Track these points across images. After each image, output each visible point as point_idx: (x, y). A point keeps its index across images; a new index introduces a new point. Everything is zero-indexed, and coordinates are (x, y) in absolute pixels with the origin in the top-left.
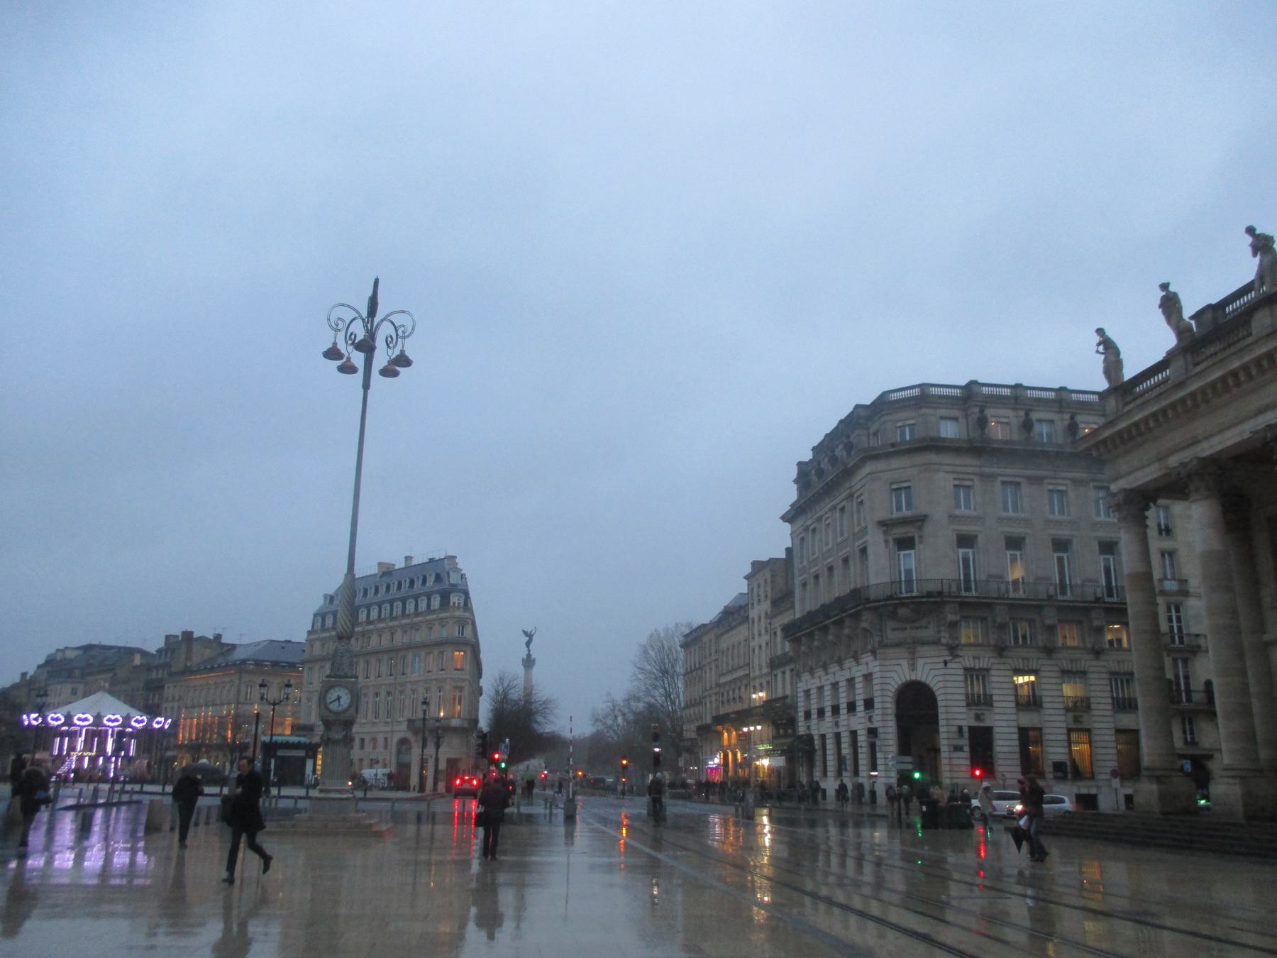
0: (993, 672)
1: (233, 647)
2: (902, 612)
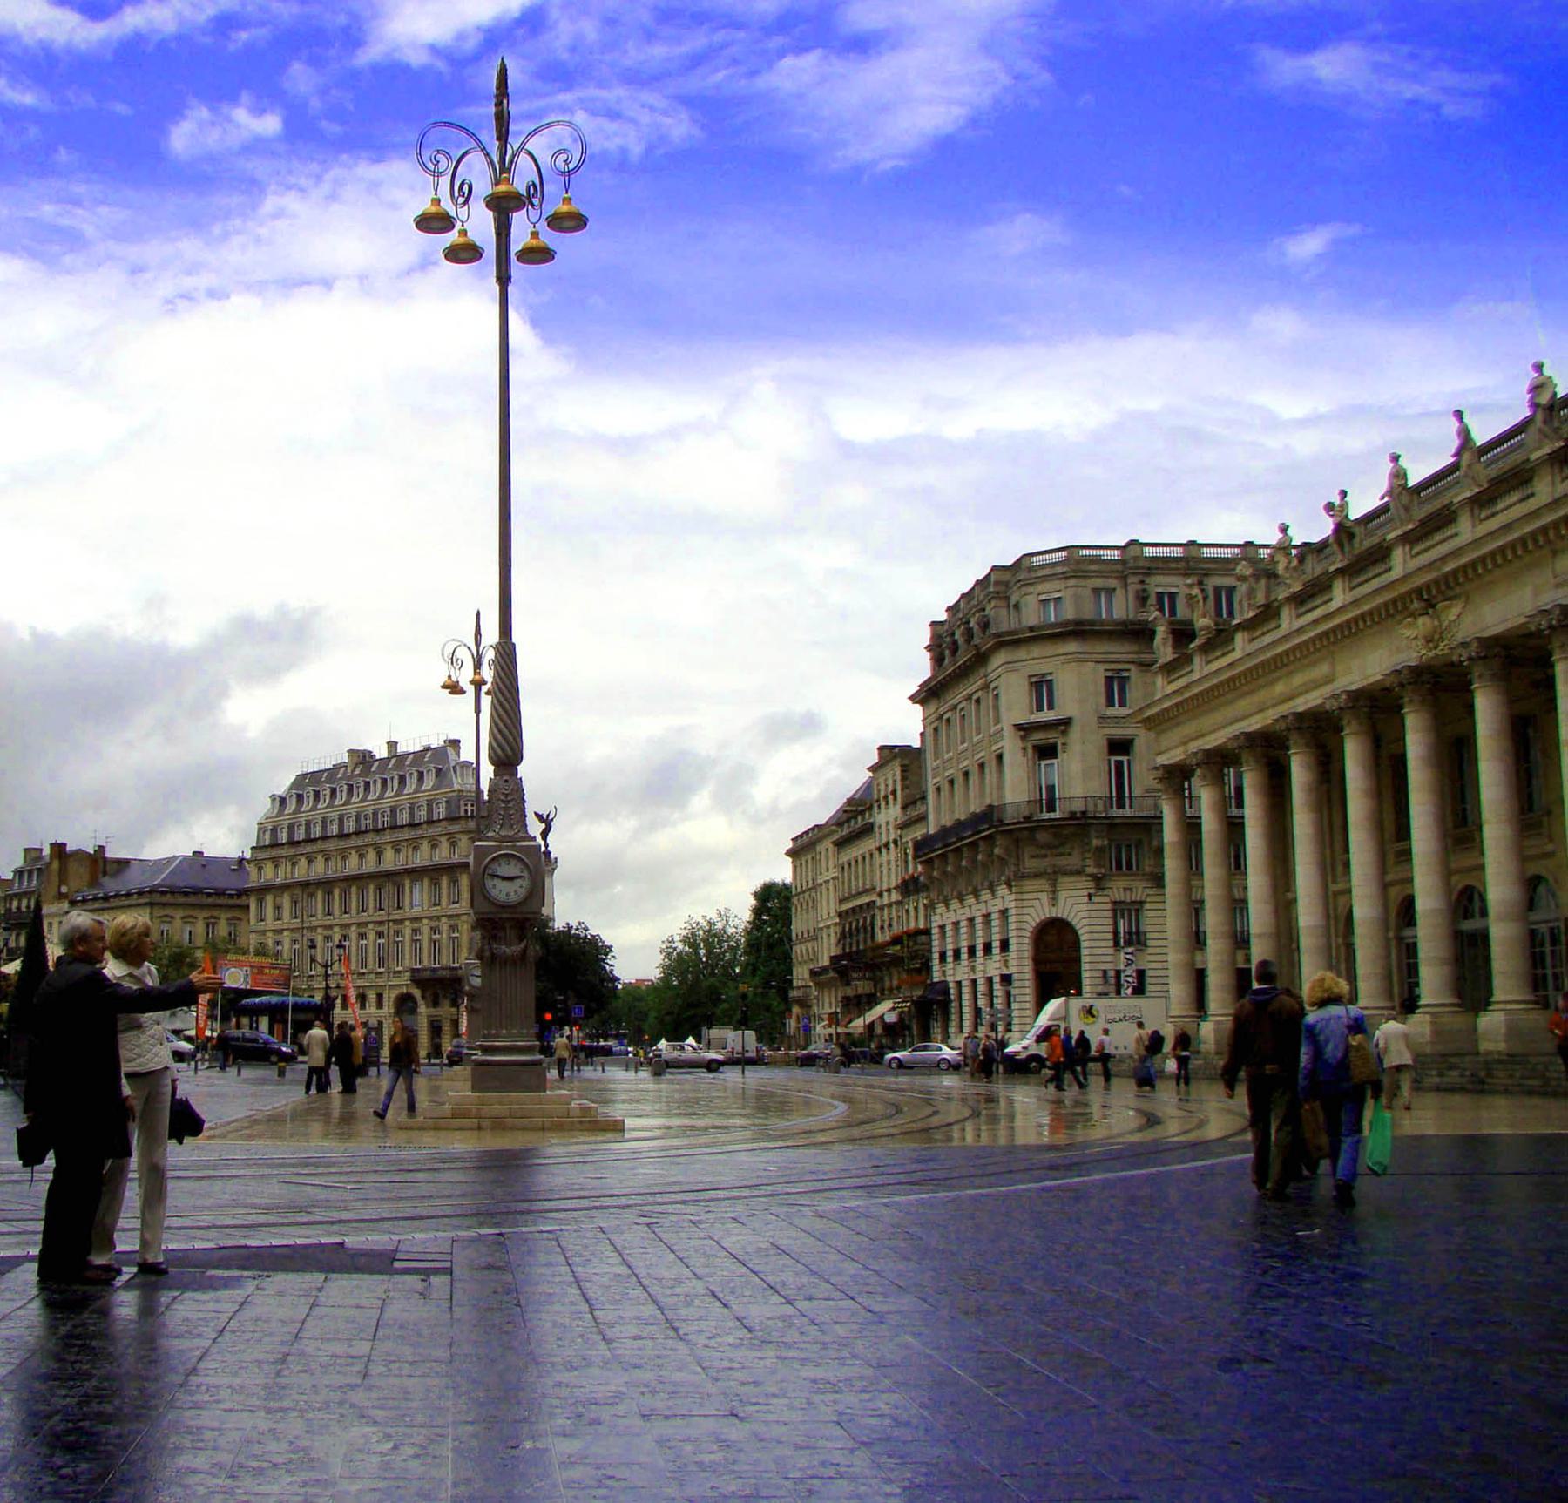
0: (1147, 906)
1: (124, 864)
2: (1042, 837)
